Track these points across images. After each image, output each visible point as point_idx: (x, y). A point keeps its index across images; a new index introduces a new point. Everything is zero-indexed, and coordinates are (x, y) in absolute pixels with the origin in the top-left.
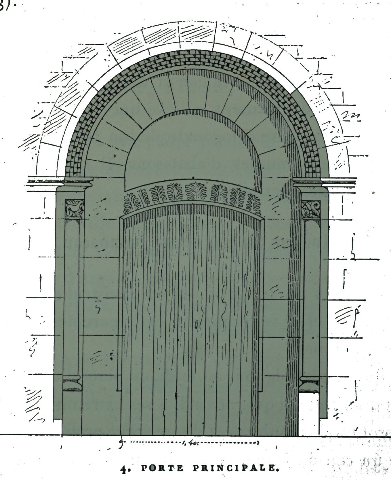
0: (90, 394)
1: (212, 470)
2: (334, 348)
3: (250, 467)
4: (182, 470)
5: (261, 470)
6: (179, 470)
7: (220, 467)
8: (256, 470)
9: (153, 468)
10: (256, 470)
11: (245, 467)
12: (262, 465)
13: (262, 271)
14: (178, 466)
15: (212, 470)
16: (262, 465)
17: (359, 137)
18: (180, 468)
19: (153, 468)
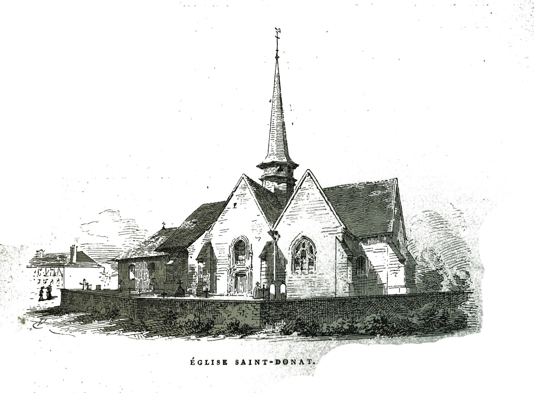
0: (475, 327)
1: (250, 364)
2: (217, 223)
3: (240, 362)
4: (226, 364)
5: (206, 364)
6: (224, 364)
7: (244, 363)
8: (245, 364)
9: (285, 362)
10: (245, 364)
11: (218, 362)
12: (206, 361)
13: (337, 216)
14: (224, 360)
15: (250, 364)
16: (206, 361)
17: (278, 31)
18: (225, 362)
19: (285, 362)
